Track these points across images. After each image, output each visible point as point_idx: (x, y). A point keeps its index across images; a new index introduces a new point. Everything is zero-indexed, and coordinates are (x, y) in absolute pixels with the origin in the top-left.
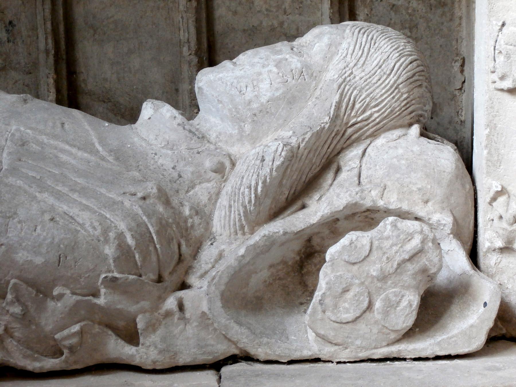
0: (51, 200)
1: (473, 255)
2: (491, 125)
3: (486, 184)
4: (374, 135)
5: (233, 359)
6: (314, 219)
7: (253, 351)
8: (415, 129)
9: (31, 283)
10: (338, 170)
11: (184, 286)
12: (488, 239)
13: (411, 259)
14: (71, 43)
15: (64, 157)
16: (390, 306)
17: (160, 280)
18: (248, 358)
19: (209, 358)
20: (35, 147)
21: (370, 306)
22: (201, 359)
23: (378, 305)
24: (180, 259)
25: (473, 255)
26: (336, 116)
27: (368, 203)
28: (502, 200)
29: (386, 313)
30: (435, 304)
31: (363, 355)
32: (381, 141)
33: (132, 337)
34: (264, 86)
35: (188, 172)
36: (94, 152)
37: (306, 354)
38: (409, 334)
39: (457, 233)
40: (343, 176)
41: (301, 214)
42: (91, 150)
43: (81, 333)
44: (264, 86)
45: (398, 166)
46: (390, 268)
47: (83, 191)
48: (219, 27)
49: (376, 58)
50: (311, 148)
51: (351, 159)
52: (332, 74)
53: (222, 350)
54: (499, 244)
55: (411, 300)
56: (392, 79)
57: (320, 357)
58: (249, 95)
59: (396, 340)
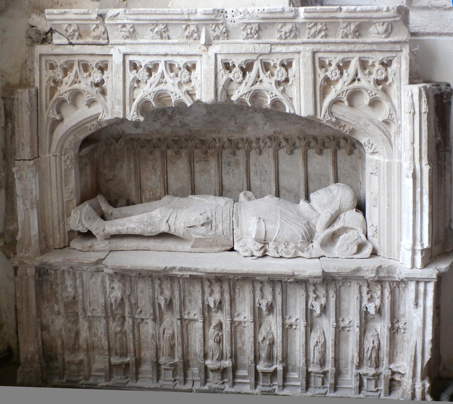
0: (289, 225)
1: (366, 236)
2: (370, 212)
3: (369, 224)
4: (346, 211)
5: (322, 257)
6: (336, 229)
7: (326, 255)
8: (354, 210)
9: (286, 242)
10: (340, 218)
11: (312, 242)
12: (369, 234)
13: (356, 240)
14: (278, 175)
15: (289, 214)
16: (352, 249)
17: (308, 241)
18: (325, 256)
19: (318, 256)
20: (283, 212)
21: (348, 248)
22: (316, 257)
23: (349, 248)
24: (311, 236)
25: (366, 236)
26: (340, 207)
27: (346, 226)
28: (372, 227)
29: (351, 250)
30: (361, 247)
31: (347, 257)
32: (348, 212)
33: (303, 251)
34: (325, 200)
35: (311, 217)
36: (294, 213)
37: (336, 257)
38: (355, 254)
39: (363, 233)
40: (341, 219)
41: (333, 227)
42: (294, 213)
43: (295, 251)
44: (325, 200)
45: (351, 217)
46: (352, 241)
47: (294, 223)
48: (308, 173)
49: (347, 195)
50: (335, 214)
51: (342, 216)
52: (338, 198)
53: (320, 255)
54: (372, 235)
55: (356, 248)
56: (350, 200)
57: (167, 52)
58: (322, 201)
59: (330, 223)
